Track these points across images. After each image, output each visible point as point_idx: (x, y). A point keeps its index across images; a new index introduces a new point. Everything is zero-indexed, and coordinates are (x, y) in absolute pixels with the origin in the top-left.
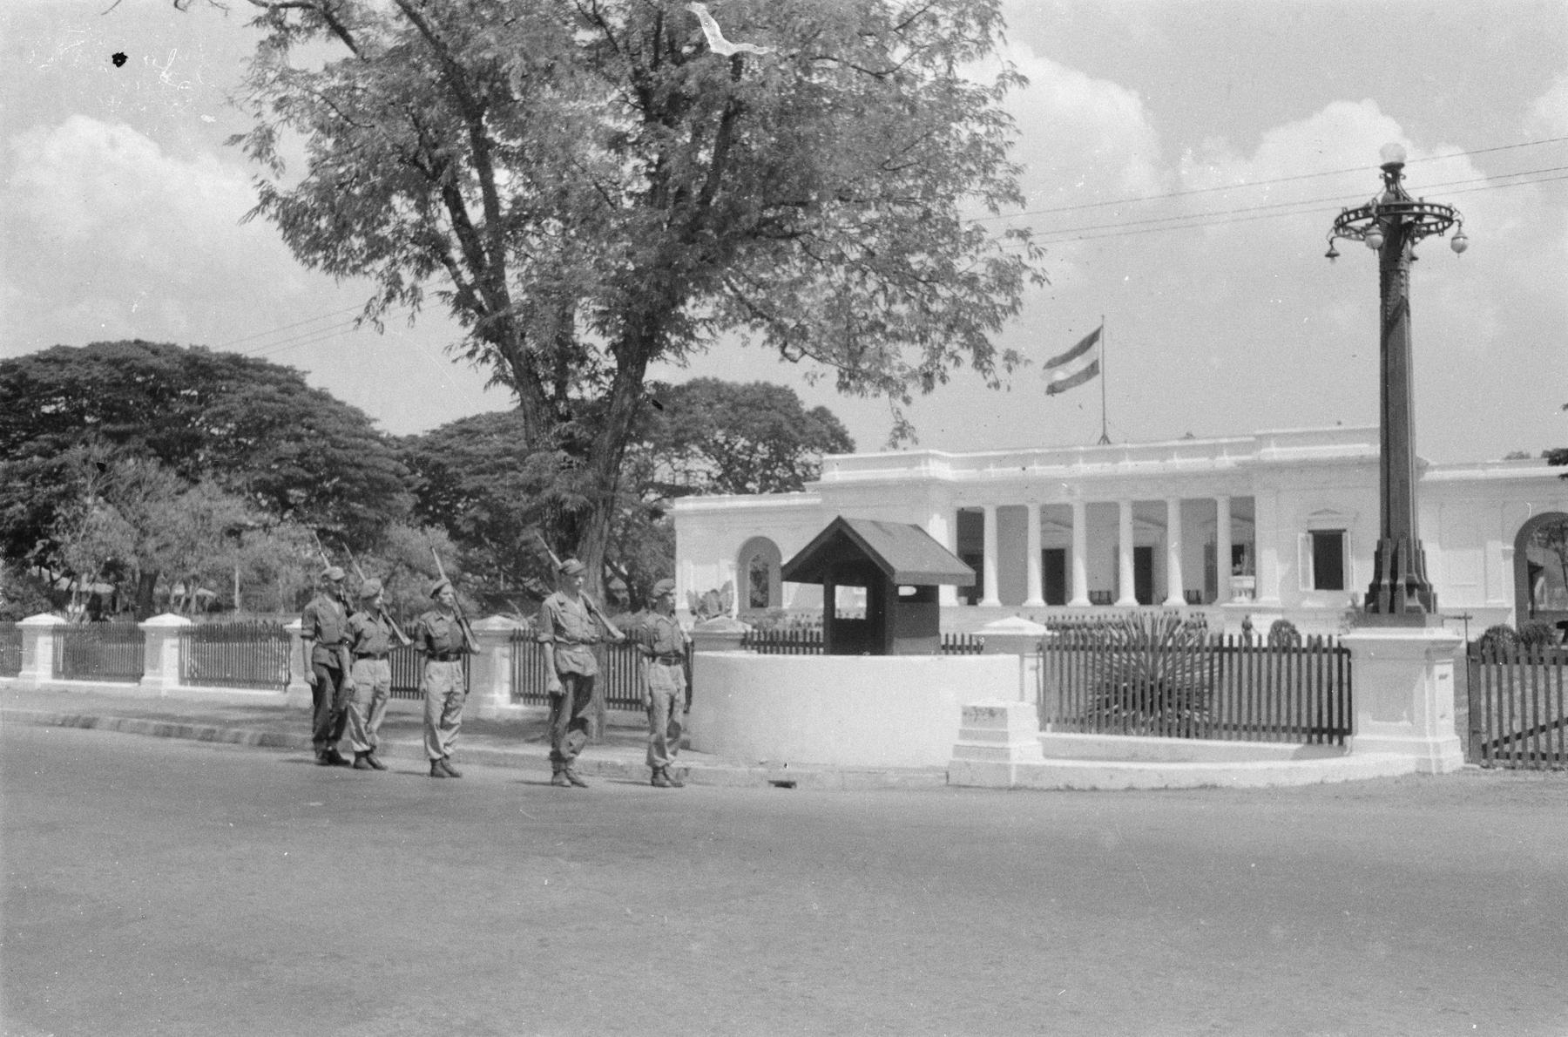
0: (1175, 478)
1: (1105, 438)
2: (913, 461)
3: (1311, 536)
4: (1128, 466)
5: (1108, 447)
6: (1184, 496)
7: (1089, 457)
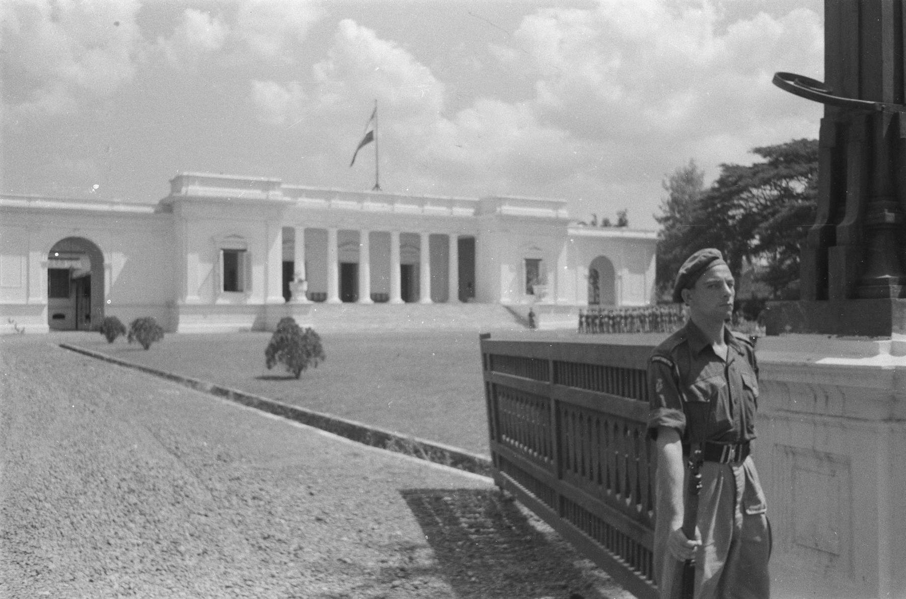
0: (427, 218)
1: (377, 186)
5: (379, 192)
6: (434, 232)
7: (374, 199)
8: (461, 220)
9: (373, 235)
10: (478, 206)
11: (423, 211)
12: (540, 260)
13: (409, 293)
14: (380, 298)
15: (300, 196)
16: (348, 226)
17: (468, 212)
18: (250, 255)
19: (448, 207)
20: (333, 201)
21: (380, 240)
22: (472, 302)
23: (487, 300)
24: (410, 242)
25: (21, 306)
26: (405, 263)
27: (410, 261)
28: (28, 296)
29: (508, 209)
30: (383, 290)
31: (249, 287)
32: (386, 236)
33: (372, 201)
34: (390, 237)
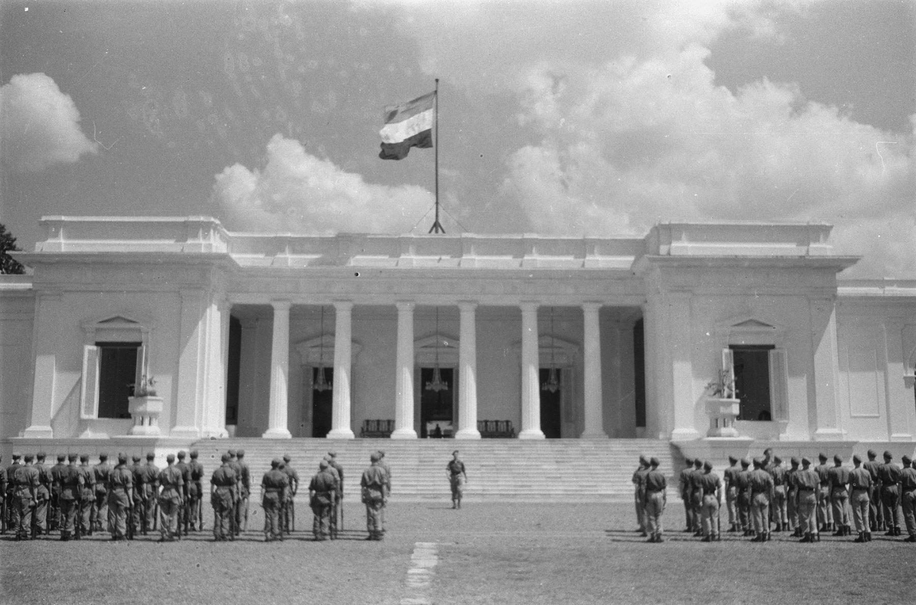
1: (436, 225)
2: (186, 230)
3: (732, 351)
4: (475, 261)
6: (546, 301)
8: (296, 275)
9: (484, 315)
10: (639, 247)
11: (521, 265)
12: (773, 347)
13: (554, 424)
14: (498, 429)
15: (282, 251)
16: (565, 298)
17: (624, 262)
18: (779, 357)
19: (515, 256)
20: (589, 258)
21: (499, 324)
22: (642, 436)
23: (654, 436)
24: (560, 325)
25: (886, 443)
26: (546, 367)
27: (561, 361)
28: (890, 433)
29: (684, 247)
30: (375, 414)
31: (783, 411)
32: (576, 315)
33: (418, 253)
34: (396, 316)
